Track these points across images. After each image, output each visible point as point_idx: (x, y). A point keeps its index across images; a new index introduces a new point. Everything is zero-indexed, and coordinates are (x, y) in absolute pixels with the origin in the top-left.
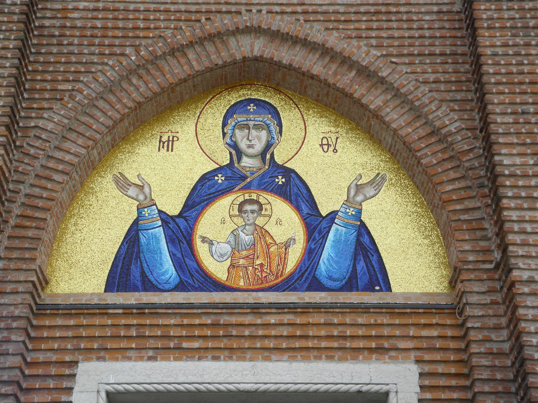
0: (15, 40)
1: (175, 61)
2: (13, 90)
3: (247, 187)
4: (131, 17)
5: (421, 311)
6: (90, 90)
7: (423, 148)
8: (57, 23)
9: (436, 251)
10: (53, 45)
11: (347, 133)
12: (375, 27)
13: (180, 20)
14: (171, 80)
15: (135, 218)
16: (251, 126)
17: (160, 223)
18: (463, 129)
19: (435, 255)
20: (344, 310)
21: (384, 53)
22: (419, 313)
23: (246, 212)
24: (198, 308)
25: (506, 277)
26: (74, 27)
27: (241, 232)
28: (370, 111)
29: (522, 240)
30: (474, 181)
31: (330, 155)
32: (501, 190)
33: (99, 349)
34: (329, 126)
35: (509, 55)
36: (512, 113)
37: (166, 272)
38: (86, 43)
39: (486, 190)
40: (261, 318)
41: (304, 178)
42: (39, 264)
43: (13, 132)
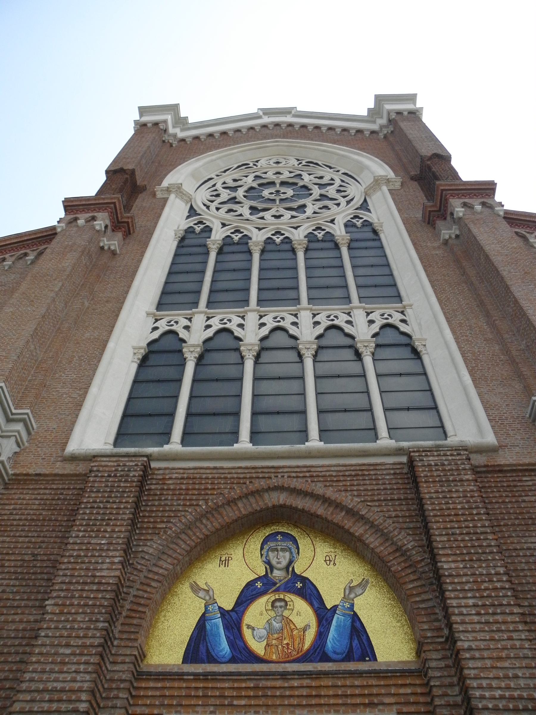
0: (133, 497)
1: (230, 509)
2: (129, 528)
3: (277, 590)
4: (203, 482)
5: (398, 674)
7: (391, 560)
8: (159, 487)
10: (155, 500)
11: (342, 552)
12: (355, 484)
13: (233, 483)
14: (228, 521)
15: (203, 612)
17: (219, 615)
18: (416, 546)
20: (345, 676)
21: (362, 499)
22: (397, 676)
23: (276, 607)
24: (244, 675)
25: (454, 647)
26: (168, 489)
27: (273, 622)
28: (356, 537)
29: (461, 620)
32: (444, 586)
33: (177, 705)
35: (440, 498)
37: (223, 649)
38: (175, 498)
39: (435, 587)
40: (287, 682)
41: (314, 583)
43: (128, 554)
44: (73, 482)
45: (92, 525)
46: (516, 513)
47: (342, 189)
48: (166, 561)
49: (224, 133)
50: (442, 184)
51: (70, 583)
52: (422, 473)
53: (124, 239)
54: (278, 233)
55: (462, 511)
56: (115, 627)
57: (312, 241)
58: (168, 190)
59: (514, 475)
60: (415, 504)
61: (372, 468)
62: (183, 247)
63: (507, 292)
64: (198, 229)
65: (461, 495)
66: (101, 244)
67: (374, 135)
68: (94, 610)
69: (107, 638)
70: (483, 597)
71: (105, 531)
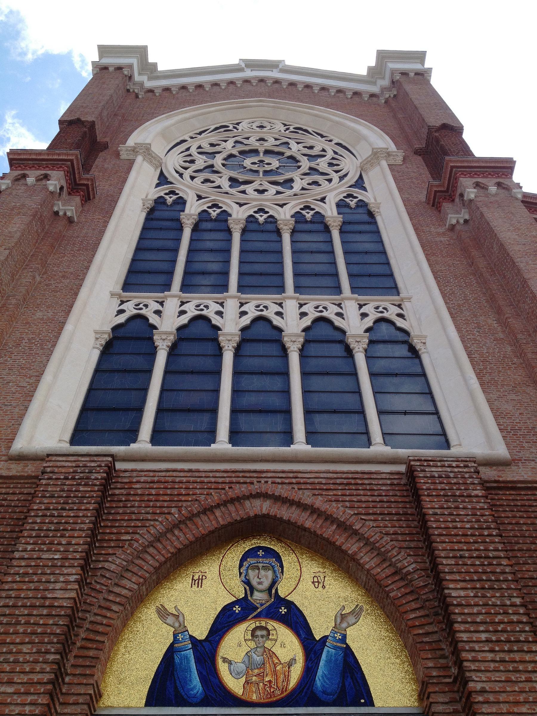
0: (94, 503)
1: (206, 518)
2: (89, 539)
6: (144, 540)
7: (390, 585)
8: (124, 492)
9: (406, 669)
10: (120, 507)
11: (332, 573)
13: (211, 489)
14: (203, 532)
15: (171, 642)
16: (260, 568)
17: (190, 646)
19: (406, 672)
21: (356, 512)
23: (257, 637)
25: (464, 689)
29: (473, 657)
30: (430, 610)
31: (320, 590)
34: (318, 568)
35: (445, 515)
36: (453, 557)
37: (195, 687)
39: (441, 618)
42: (96, 679)
43: (86, 572)
44: (19, 486)
45: (43, 537)
46: (532, 537)
47: (335, 162)
48: (130, 580)
49: (199, 86)
50: (452, 161)
51: (15, 606)
52: (423, 484)
53: (82, 204)
54: (261, 210)
55: (471, 531)
56: (67, 660)
57: (299, 222)
58: (134, 150)
59: (529, 493)
60: (415, 521)
61: (366, 476)
62: (152, 219)
63: (523, 287)
64: (170, 200)
65: (470, 513)
66: (56, 209)
67: (374, 99)
68: (44, 640)
69: (58, 674)
70: (496, 631)
71: (59, 544)
